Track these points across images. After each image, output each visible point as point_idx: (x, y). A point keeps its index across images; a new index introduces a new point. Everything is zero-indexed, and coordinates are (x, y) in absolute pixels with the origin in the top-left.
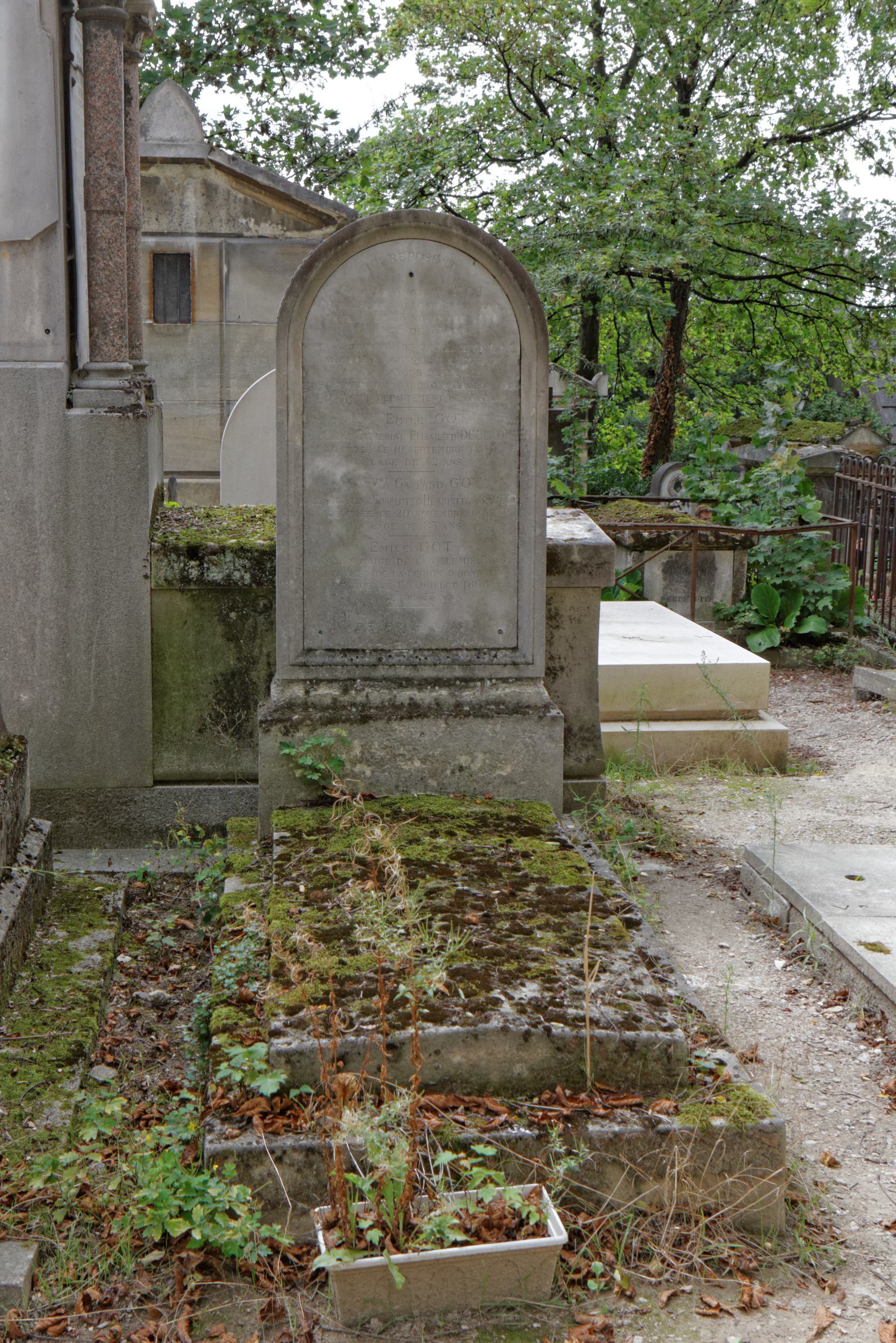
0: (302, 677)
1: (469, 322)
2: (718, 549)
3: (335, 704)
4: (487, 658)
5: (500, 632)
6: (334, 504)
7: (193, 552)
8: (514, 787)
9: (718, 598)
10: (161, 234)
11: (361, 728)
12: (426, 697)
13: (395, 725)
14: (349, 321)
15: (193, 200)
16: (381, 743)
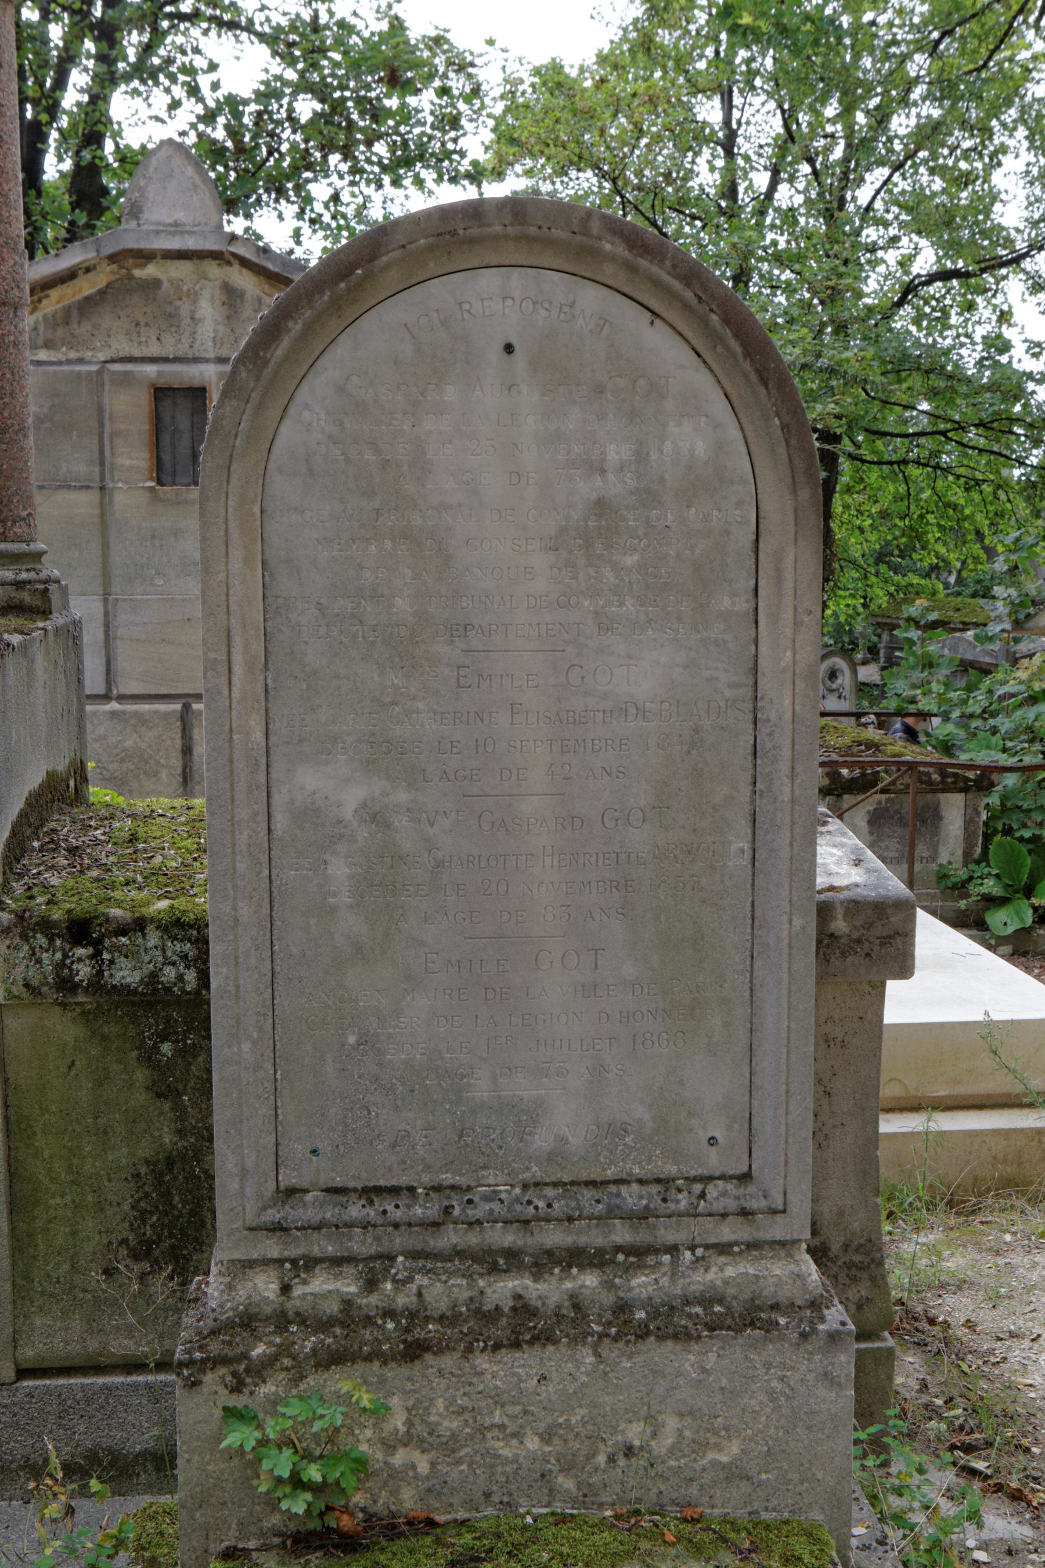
0: (274, 1253)
1: (641, 456)
2: (944, 791)
3: (349, 1317)
4: (683, 1201)
5: (712, 1141)
6: (339, 870)
7: (80, 930)
8: (745, 1487)
9: (943, 859)
10: (166, 360)
11: (405, 1370)
12: (549, 1291)
13: (482, 1362)
14: (369, 456)
15: (208, 310)
16: (452, 1401)
